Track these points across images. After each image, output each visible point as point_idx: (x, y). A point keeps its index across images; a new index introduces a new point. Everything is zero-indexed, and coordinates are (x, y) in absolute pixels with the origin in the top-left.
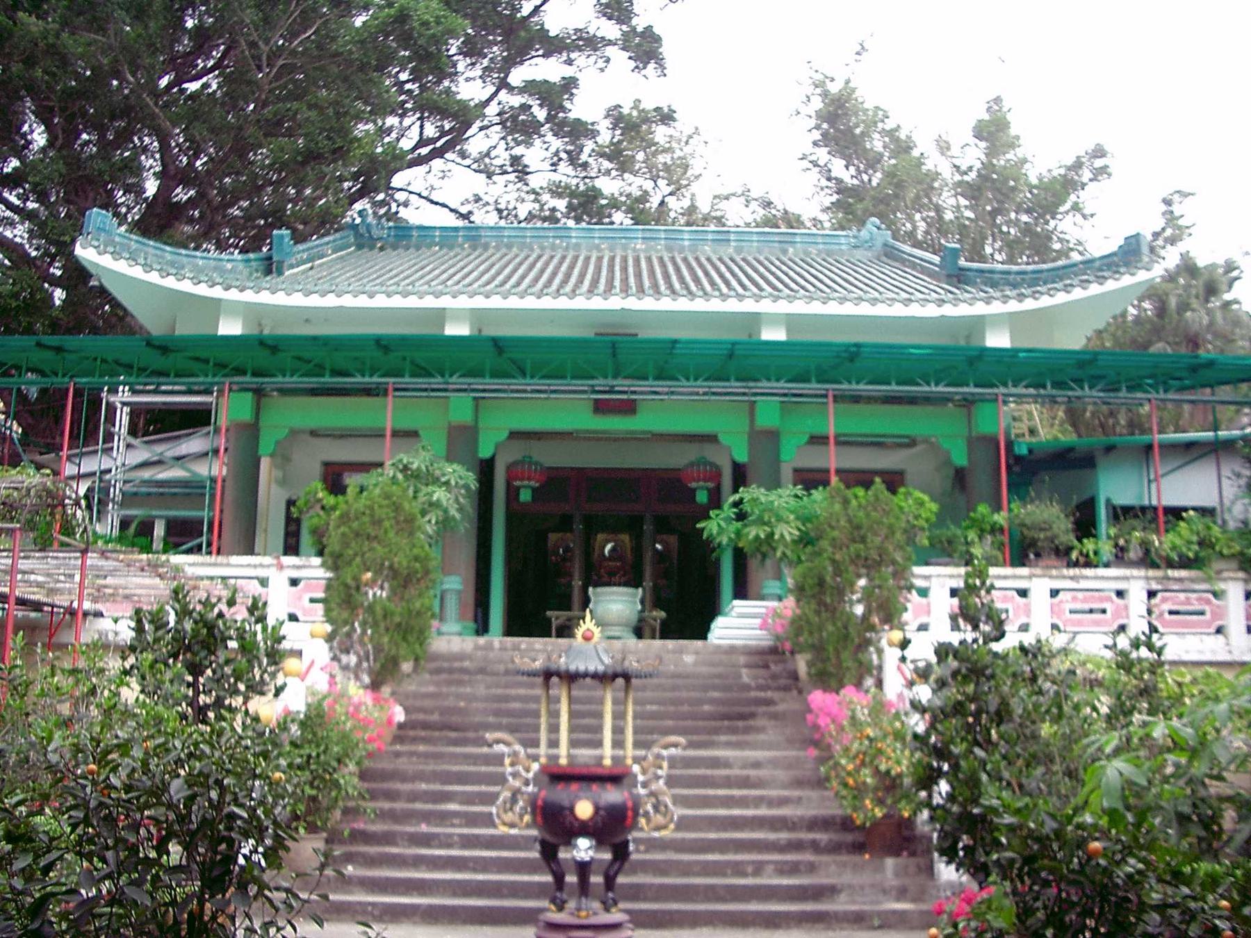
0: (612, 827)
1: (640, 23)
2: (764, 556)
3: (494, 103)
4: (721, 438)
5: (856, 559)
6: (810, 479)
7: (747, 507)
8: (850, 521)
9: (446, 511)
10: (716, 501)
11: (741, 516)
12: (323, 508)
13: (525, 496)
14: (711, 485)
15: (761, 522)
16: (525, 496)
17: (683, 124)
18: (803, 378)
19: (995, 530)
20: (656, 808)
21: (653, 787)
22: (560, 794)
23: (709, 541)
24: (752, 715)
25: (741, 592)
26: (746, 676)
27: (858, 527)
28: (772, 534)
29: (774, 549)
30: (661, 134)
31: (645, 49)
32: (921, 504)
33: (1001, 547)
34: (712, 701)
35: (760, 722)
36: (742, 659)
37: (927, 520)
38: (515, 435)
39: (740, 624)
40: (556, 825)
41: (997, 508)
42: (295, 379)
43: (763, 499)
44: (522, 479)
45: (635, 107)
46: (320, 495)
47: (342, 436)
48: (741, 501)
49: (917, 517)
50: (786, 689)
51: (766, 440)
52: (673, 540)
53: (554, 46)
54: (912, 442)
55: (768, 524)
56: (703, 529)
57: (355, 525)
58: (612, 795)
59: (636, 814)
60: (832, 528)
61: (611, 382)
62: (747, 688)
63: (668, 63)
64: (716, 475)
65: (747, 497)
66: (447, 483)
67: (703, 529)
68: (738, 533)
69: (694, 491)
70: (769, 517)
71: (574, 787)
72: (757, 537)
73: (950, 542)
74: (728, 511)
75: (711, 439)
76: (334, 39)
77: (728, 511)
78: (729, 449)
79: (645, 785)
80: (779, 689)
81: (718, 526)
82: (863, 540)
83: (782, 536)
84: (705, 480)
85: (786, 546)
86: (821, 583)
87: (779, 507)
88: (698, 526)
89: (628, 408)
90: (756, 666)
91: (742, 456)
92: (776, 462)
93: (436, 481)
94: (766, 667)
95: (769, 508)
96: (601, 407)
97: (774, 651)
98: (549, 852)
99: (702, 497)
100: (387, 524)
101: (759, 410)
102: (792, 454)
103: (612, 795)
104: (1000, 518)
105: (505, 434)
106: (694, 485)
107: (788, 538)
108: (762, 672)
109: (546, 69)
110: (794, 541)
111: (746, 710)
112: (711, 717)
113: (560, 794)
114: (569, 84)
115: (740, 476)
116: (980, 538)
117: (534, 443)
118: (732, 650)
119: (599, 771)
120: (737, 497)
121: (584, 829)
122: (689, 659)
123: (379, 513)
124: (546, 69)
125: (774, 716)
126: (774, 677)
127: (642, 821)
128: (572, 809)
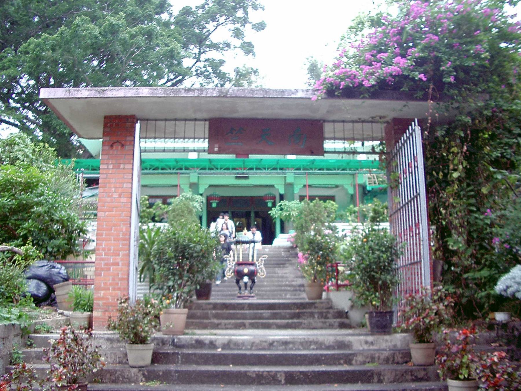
0: (252, 275)
1: (247, 40)
2: (288, 221)
3: (194, 67)
4: (275, 186)
5: (311, 220)
6: (302, 198)
7: (283, 207)
8: (309, 209)
9: (197, 209)
10: (274, 205)
11: (281, 209)
12: (161, 209)
13: (214, 205)
14: (272, 201)
15: (287, 211)
16: (214, 205)
17: (261, 72)
18: (298, 169)
19: (354, 212)
20: (261, 271)
21: (261, 266)
22: (240, 268)
23: (272, 217)
24: (285, 264)
25: (283, 231)
26: (283, 254)
27: (312, 211)
28: (290, 214)
29: (291, 218)
30: (253, 77)
31: (248, 48)
32: (333, 205)
33: (357, 217)
34: (274, 261)
35: (287, 265)
36: (282, 250)
37: (335, 210)
38: (211, 186)
39: (282, 240)
40: (239, 275)
41: (355, 206)
42: (150, 171)
43: (287, 204)
44: (213, 200)
45: (244, 66)
46: (160, 205)
47: (152, 187)
48: (281, 205)
49: (332, 209)
50: (295, 257)
51: (289, 186)
52: (260, 220)
53: (215, 46)
54: (337, 186)
55: (289, 211)
56: (270, 214)
57: (177, 212)
58: (252, 268)
59: (257, 273)
60: (305, 211)
61: (243, 171)
62: (283, 257)
63: (256, 54)
64: (274, 198)
65: (283, 204)
66: (197, 201)
67: (270, 214)
68: (281, 214)
69: (267, 203)
70: (290, 209)
71: (243, 266)
72: (286, 215)
73: (341, 216)
74: (278, 208)
75: (272, 186)
76: (147, 56)
77: (278, 208)
78: (278, 189)
79: (259, 266)
80: (292, 257)
81: (274, 212)
82: (313, 214)
83: (293, 215)
84: (271, 199)
85: (294, 217)
86: (302, 226)
87: (293, 206)
88: (269, 212)
89: (247, 178)
90: (286, 251)
91: (282, 192)
92: (293, 193)
93: (194, 200)
94: (289, 251)
95: (289, 207)
96: (237, 178)
97: (292, 248)
98: (238, 282)
99: (270, 205)
100: (186, 212)
101: (287, 178)
102: (297, 190)
103: (252, 268)
104: (356, 209)
105: (208, 186)
106: (267, 201)
107: (295, 215)
108: (288, 253)
109: (213, 54)
110: (453, 317)
111: (283, 262)
112: (274, 264)
113: (240, 268)
114: (222, 62)
115: (282, 197)
116: (351, 214)
117: (217, 189)
118: (279, 247)
119: (248, 262)
120: (280, 204)
121: (246, 275)
122: (267, 250)
123: (183, 209)
124: (213, 54)
125: (291, 264)
126: (291, 254)
127: (258, 274)
128: (243, 271)
